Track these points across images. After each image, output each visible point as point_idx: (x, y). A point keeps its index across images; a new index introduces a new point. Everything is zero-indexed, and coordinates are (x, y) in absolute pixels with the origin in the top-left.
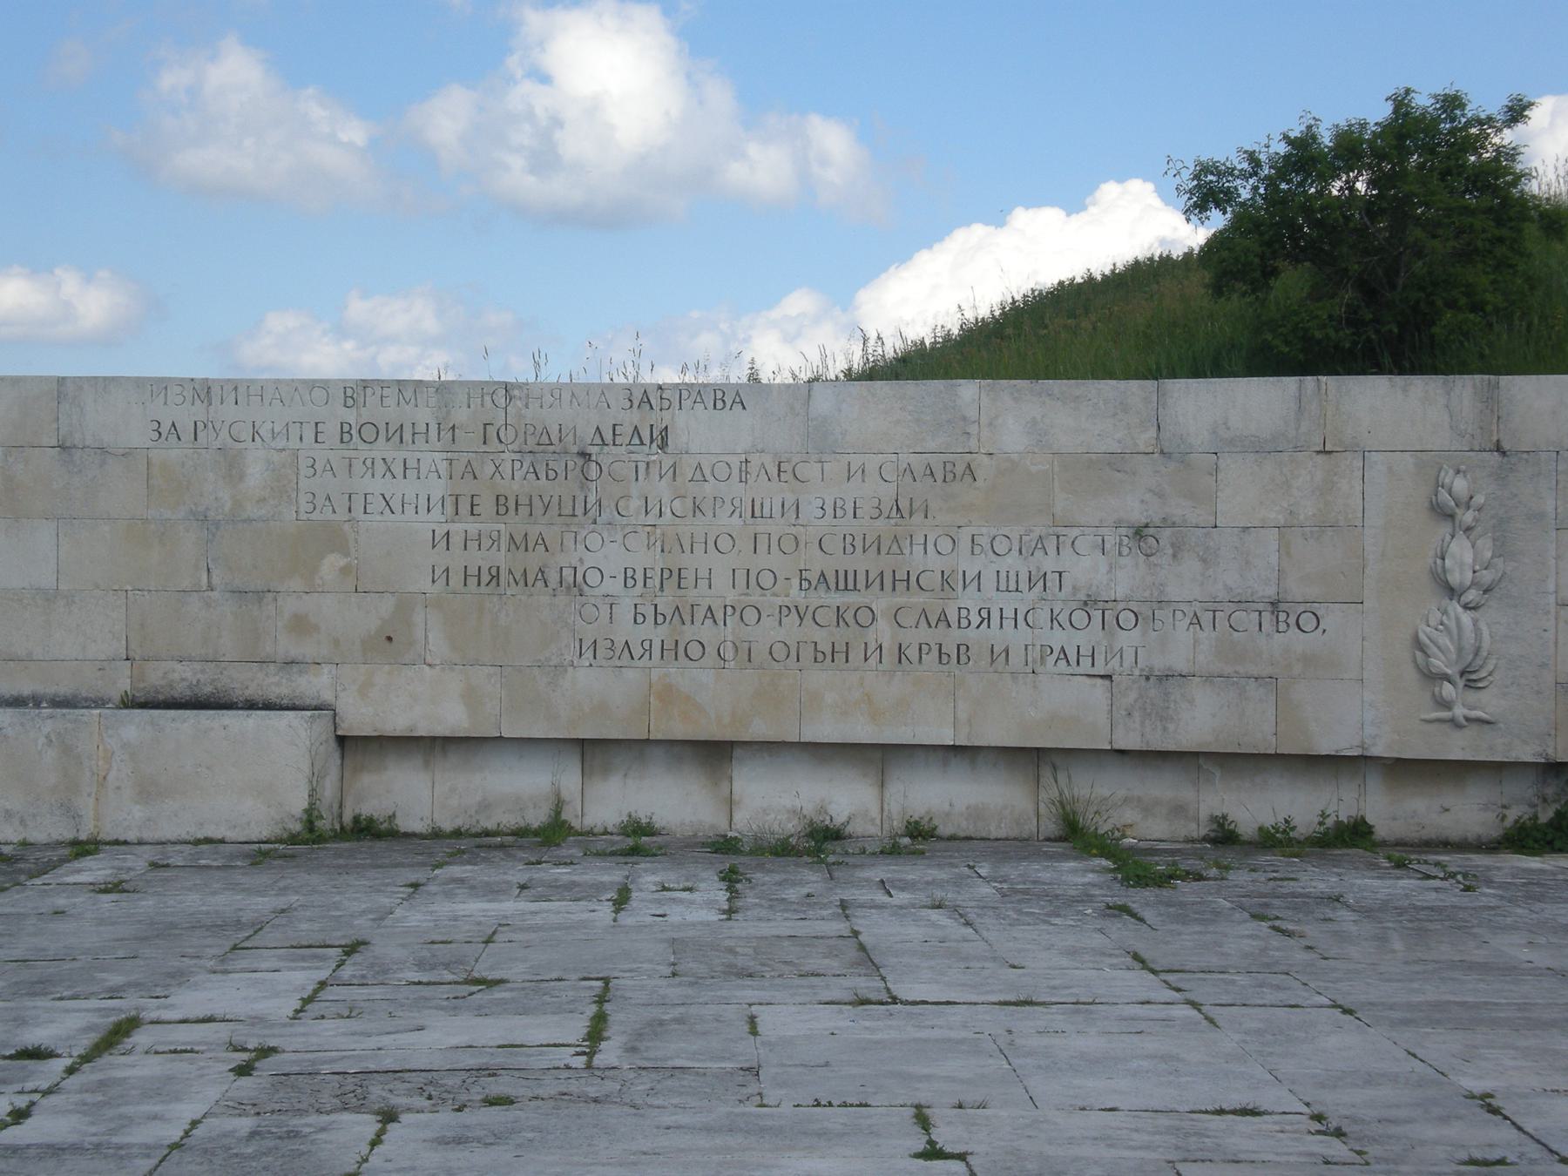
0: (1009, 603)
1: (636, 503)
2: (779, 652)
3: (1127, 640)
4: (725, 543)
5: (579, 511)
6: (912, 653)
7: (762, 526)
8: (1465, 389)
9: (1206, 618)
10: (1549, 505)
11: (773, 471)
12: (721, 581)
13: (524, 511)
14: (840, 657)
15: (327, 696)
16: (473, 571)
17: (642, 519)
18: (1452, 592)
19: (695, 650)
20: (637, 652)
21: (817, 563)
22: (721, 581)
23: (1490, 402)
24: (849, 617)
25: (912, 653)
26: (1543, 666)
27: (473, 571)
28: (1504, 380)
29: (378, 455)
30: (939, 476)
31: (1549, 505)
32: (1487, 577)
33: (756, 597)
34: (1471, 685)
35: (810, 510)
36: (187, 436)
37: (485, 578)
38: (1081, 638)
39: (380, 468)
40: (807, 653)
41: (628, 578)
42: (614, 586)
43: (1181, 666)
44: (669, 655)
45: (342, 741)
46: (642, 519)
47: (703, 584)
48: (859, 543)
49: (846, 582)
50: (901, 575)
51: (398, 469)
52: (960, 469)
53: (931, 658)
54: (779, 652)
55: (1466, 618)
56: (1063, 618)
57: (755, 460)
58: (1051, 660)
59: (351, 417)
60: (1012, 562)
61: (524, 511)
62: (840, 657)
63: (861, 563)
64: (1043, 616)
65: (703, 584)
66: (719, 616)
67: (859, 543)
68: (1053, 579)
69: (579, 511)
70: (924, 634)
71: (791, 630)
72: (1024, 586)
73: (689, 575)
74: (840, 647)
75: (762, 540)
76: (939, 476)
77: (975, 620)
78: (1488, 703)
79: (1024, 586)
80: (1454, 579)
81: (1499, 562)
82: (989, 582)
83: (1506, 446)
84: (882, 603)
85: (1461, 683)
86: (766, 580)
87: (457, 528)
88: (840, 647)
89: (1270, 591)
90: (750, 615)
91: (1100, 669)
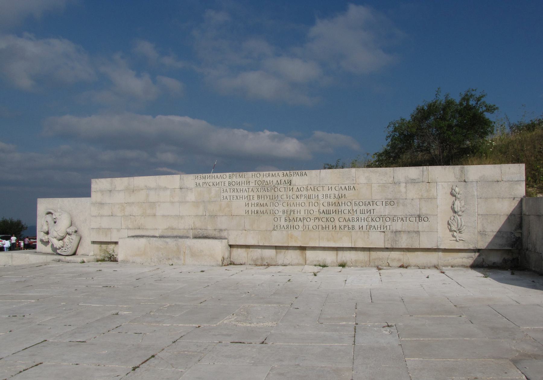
0: (363, 216)
1: (285, 196)
2: (315, 227)
3: (388, 224)
4: (303, 204)
5: (274, 198)
6: (343, 227)
7: (311, 200)
8: (457, 168)
9: (404, 219)
10: (476, 194)
11: (313, 189)
12: (302, 213)
13: (263, 198)
14: (327, 228)
15: (227, 237)
16: (253, 211)
17: (286, 199)
18: (455, 212)
19: (297, 227)
20: (286, 227)
21: (332, 200)
22: (302, 213)
23: (258, 243)
24: (329, 219)
25: (343, 227)
26: (475, 228)
27: (253, 211)
28: (465, 166)
29: (235, 188)
30: (347, 189)
31: (476, 194)
32: (463, 209)
33: (310, 216)
34: (460, 232)
35: (320, 197)
36: (201, 185)
37: (286, 227)
38: (378, 224)
39: (236, 190)
40: (320, 227)
41: (284, 212)
42: (281, 214)
43: (399, 229)
44: (292, 228)
45: (231, 246)
46: (286, 199)
47: (299, 213)
48: (331, 204)
49: (328, 212)
50: (340, 211)
51: (239, 191)
52: (352, 188)
53: (346, 229)
54: (315, 227)
55: (459, 218)
56: (374, 219)
57: (309, 187)
58: (372, 228)
59: (230, 180)
60: (363, 207)
61: (263, 198)
62: (327, 228)
63: (332, 208)
64: (370, 219)
65: (299, 213)
66: (302, 220)
67: (331, 204)
68: (372, 211)
69: (274, 198)
70: (344, 223)
71: (317, 223)
72: (366, 212)
73: (296, 211)
74: (327, 226)
75: (306, 211)
76: (347, 189)
77: (356, 220)
78: (464, 236)
79: (366, 212)
80: (456, 210)
81: (466, 206)
82: (358, 212)
83: (466, 180)
84: (336, 217)
85: (458, 232)
86: (312, 212)
87: (250, 202)
88: (327, 226)
89: (418, 213)
90: (308, 220)
91: (382, 230)
